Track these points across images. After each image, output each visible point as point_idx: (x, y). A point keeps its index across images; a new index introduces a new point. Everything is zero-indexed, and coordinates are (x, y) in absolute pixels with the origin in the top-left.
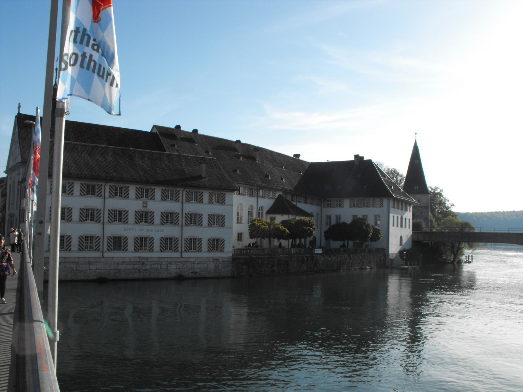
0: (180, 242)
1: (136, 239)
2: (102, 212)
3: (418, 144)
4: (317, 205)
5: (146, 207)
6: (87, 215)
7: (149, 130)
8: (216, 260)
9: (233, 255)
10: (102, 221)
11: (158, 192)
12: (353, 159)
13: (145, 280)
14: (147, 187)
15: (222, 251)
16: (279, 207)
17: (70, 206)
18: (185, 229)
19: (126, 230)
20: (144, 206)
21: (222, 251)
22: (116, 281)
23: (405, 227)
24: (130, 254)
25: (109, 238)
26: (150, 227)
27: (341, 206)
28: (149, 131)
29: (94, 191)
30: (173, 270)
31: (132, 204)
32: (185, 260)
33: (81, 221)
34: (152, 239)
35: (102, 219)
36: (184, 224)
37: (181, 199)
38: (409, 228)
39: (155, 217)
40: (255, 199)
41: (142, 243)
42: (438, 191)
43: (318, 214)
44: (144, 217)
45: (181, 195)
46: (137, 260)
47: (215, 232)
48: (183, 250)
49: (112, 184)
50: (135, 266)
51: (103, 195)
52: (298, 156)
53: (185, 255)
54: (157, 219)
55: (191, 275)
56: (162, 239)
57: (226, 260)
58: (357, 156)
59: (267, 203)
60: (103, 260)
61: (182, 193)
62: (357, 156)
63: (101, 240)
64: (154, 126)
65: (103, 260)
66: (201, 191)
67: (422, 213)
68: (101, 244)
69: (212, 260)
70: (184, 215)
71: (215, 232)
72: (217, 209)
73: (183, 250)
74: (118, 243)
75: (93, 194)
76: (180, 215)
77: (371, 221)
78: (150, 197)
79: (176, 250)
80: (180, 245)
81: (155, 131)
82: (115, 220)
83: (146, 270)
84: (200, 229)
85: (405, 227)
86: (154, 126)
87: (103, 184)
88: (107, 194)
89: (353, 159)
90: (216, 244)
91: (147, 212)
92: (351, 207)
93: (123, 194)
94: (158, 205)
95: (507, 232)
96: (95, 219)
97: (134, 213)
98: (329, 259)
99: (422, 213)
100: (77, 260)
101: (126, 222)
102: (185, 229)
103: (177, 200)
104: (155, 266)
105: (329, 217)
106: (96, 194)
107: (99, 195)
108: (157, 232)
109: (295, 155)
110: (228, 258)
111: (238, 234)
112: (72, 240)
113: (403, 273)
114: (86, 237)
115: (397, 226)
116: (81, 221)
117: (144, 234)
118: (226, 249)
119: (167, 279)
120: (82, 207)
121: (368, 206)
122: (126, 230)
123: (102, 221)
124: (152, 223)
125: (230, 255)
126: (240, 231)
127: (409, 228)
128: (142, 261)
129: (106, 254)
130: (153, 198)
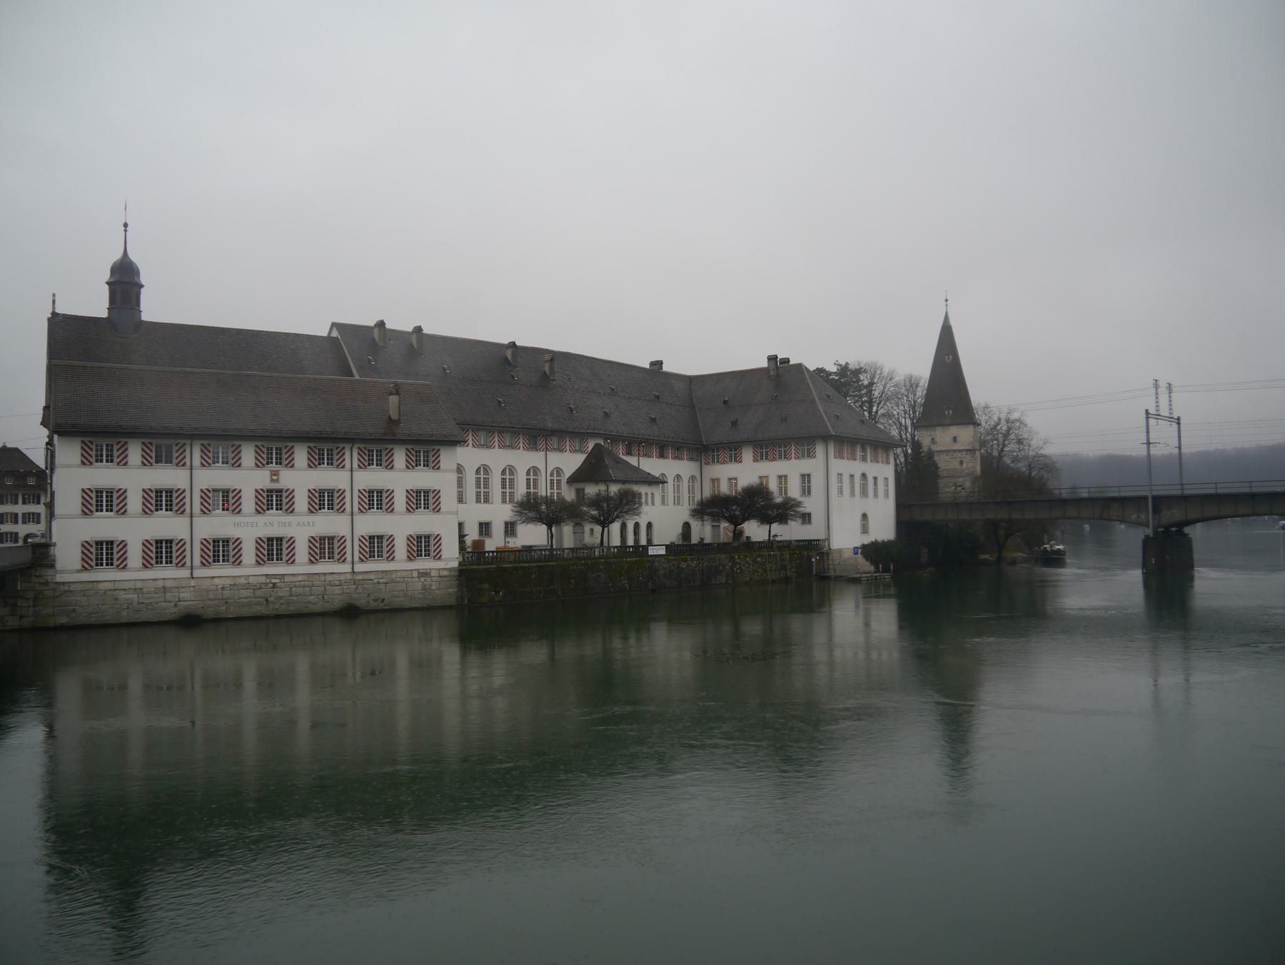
0: (348, 544)
1: (259, 541)
2: (187, 494)
3: (952, 323)
4: (691, 459)
5: (277, 481)
6: (99, 502)
7: (323, 331)
8: (424, 574)
9: (460, 564)
10: (188, 511)
11: (400, 457)
12: (764, 364)
13: (278, 617)
14: (279, 445)
15: (438, 557)
16: (590, 471)
17: (123, 487)
18: (359, 519)
19: (236, 525)
20: (272, 480)
21: (438, 557)
22: (218, 621)
23: (876, 495)
24: (249, 569)
25: (204, 542)
26: (238, 519)
27: (738, 459)
28: (325, 334)
29: (171, 457)
30: (337, 600)
31: (248, 477)
32: (360, 577)
33: (146, 512)
34: (291, 541)
35: (187, 507)
36: (356, 509)
37: (347, 463)
38: (887, 495)
39: (395, 500)
40: (543, 454)
41: (273, 548)
42: (1015, 416)
43: (693, 478)
44: (274, 499)
45: (347, 456)
46: (263, 580)
47: (422, 522)
48: (356, 558)
49: (362, 446)
50: (258, 593)
51: (188, 464)
52: (658, 364)
53: (360, 567)
54: (301, 502)
55: (373, 605)
56: (312, 540)
57: (446, 573)
58: (772, 359)
59: (571, 462)
60: (193, 583)
61: (351, 456)
62: (772, 359)
63: (188, 546)
64: (334, 325)
65: (193, 583)
66: (390, 447)
67: (961, 463)
68: (188, 553)
69: (415, 574)
70: (356, 494)
71: (422, 522)
72: (423, 478)
73: (356, 558)
74: (221, 550)
75: (169, 461)
76: (348, 494)
77: (773, 486)
78: (285, 463)
79: (342, 560)
80: (348, 550)
81: (335, 334)
82: (371, 506)
83: (281, 598)
84: (389, 517)
85: (876, 495)
86: (334, 325)
87: (188, 442)
88: (197, 461)
89: (764, 364)
90: (423, 545)
91: (281, 491)
92: (755, 460)
93: (114, 457)
94: (302, 477)
95: (1247, 490)
96: (285, 507)
97: (253, 494)
98: (683, 565)
99: (961, 463)
100: (139, 585)
101: (291, 510)
102: (359, 519)
103: (341, 466)
104: (300, 590)
105: (715, 481)
106: (335, 463)
107: (181, 464)
108: (301, 527)
109: (652, 364)
110: (450, 570)
111: (481, 524)
112: (243, 545)
113: (873, 589)
114: (157, 542)
115: (853, 494)
116: (146, 512)
117: (104, 535)
118: (445, 554)
119: (324, 614)
120: (146, 487)
121: (787, 457)
122: (239, 525)
123: (188, 511)
124: (291, 510)
125: (455, 564)
126: (484, 519)
127: (887, 495)
128: (273, 583)
129: (197, 573)
130: (291, 465)
